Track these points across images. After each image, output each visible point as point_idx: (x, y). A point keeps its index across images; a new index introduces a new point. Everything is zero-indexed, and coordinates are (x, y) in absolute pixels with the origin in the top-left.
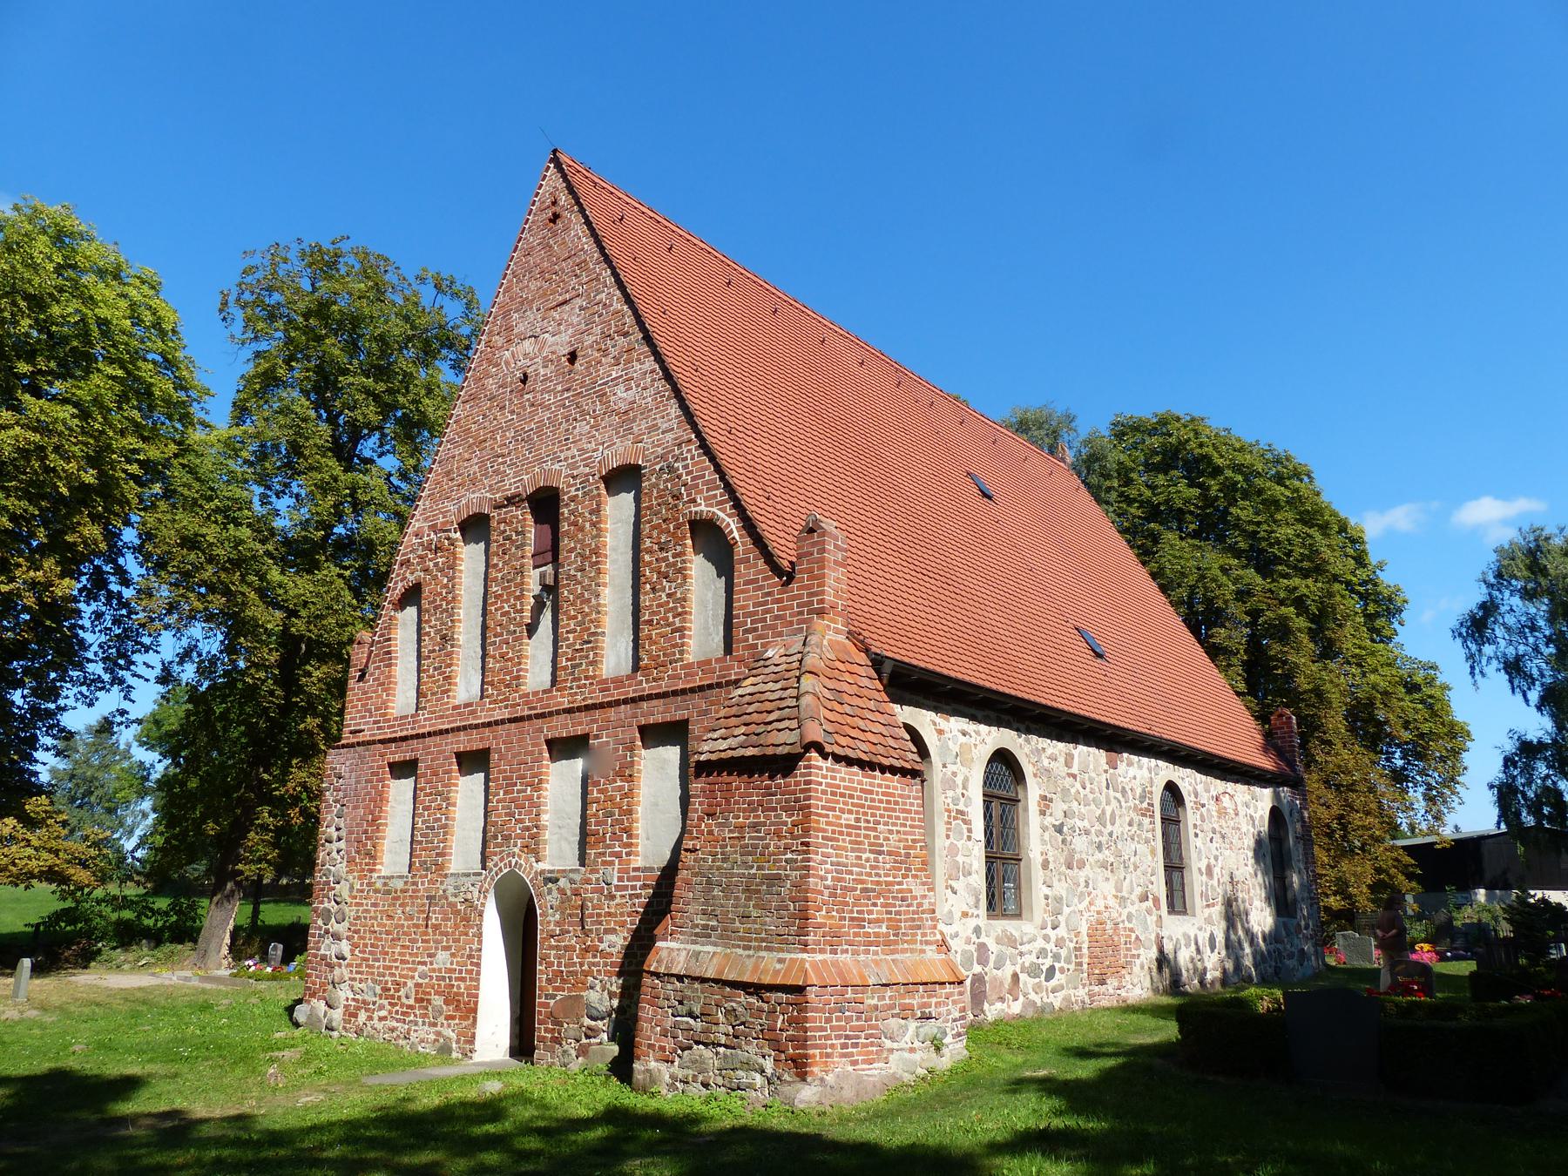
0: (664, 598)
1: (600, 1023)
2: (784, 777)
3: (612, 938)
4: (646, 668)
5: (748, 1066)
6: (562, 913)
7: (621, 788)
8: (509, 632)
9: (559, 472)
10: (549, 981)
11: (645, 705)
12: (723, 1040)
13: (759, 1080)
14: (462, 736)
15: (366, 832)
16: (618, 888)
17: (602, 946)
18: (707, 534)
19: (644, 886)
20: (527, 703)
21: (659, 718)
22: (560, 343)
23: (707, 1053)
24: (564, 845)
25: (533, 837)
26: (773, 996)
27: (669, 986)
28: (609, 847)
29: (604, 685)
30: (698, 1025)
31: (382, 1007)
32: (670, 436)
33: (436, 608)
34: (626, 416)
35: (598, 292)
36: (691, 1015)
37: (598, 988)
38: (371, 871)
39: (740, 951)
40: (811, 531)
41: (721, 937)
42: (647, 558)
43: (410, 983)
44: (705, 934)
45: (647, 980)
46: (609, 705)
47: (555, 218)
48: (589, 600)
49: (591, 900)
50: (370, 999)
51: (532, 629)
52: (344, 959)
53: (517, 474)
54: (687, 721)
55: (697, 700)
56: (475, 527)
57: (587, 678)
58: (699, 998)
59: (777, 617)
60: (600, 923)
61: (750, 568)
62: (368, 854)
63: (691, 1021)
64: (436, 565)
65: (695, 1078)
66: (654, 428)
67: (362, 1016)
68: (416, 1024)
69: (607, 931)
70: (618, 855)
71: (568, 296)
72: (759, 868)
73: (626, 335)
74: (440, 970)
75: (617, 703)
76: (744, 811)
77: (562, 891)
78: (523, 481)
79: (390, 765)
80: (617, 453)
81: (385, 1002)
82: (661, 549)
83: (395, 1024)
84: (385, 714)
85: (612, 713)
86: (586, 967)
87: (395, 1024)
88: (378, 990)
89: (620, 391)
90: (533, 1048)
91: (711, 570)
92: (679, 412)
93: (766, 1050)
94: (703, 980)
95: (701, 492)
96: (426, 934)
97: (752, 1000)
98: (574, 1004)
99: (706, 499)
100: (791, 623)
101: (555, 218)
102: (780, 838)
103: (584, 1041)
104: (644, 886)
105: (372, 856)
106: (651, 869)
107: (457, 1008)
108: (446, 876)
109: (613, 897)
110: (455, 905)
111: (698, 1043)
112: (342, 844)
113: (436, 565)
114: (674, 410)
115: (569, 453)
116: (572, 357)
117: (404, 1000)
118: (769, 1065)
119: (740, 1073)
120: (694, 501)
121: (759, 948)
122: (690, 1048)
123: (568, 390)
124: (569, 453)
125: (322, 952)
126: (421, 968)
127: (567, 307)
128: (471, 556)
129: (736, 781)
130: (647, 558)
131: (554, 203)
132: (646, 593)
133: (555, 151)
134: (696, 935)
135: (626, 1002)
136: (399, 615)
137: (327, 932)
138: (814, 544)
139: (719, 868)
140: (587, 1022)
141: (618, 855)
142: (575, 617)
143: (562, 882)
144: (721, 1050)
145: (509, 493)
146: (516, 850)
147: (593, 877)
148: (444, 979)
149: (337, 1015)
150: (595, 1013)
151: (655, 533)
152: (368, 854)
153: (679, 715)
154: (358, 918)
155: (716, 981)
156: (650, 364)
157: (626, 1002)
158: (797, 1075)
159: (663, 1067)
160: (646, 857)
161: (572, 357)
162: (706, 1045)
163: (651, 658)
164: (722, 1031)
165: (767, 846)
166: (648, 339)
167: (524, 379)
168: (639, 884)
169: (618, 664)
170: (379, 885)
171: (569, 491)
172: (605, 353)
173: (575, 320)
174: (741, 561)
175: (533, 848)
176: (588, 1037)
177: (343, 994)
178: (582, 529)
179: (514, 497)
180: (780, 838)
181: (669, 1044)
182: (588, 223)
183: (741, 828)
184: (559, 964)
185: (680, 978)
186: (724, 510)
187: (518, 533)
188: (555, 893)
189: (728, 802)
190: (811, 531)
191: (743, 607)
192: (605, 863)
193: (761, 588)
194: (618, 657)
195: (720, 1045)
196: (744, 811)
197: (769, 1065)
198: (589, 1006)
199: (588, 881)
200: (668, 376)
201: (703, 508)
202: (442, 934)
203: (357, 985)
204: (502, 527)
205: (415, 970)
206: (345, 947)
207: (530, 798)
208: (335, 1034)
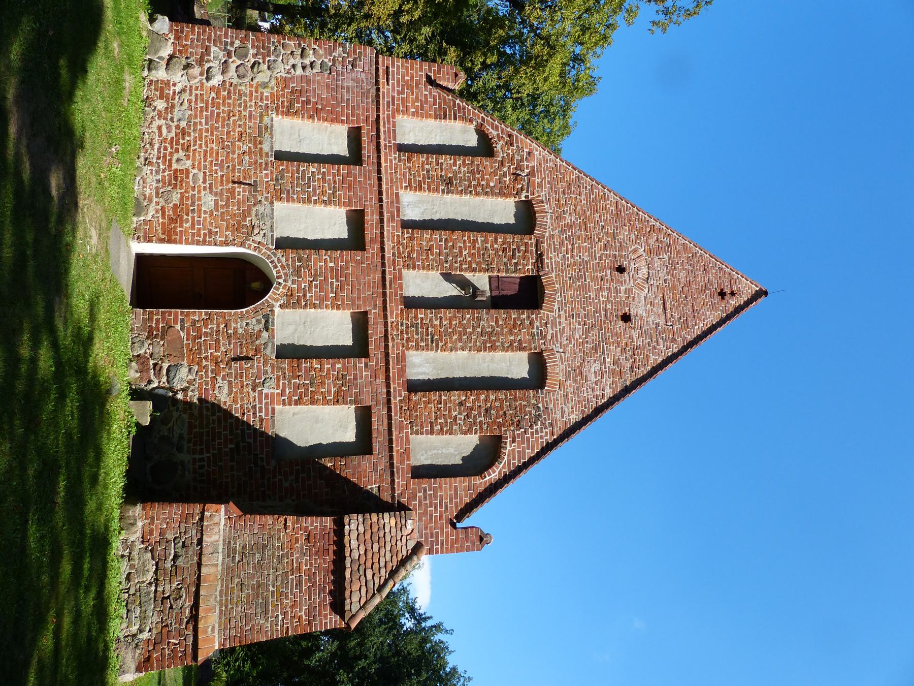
0: (454, 414)
1: (164, 379)
2: (331, 604)
3: (226, 391)
4: (410, 400)
5: (143, 618)
6: (243, 336)
7: (329, 392)
8: (447, 255)
9: (554, 308)
10: (194, 323)
11: (385, 412)
12: (160, 589)
13: (134, 629)
14: (376, 217)
15: (308, 102)
16: (261, 393)
17: (219, 379)
18: (488, 453)
19: (261, 420)
20: (395, 278)
21: (375, 427)
22: (638, 309)
23: (149, 576)
24: (291, 328)
25: (299, 300)
26: (190, 632)
27: (194, 532)
28: (290, 382)
29: (401, 358)
30: (168, 564)
31: (169, 128)
32: (559, 415)
33: (473, 173)
34: (578, 373)
35: (665, 341)
36: (176, 557)
37: (190, 377)
38: (277, 111)
39: (219, 588)
40: (481, 539)
41: (228, 568)
42: (483, 397)
43: (189, 163)
44: (230, 552)
45: (198, 508)
46: (388, 378)
47: (722, 294)
48: (460, 340)
49: (252, 367)
50: (177, 115)
51: (448, 277)
52: (208, 79)
53: (557, 263)
54: (371, 453)
55: (383, 464)
56: (527, 218)
57: (408, 339)
58: (187, 562)
59: (431, 516)
60: (236, 378)
61: (464, 488)
62: (291, 105)
63: (171, 557)
64: (505, 173)
65: (132, 567)
66: (567, 401)
67: (161, 105)
68: (157, 172)
69: (230, 383)
70: (283, 392)
71: (668, 310)
72: (273, 592)
73: (632, 369)
74: (199, 199)
75: (388, 386)
76: (310, 569)
77: (258, 336)
78: (551, 278)
79: (359, 129)
80: (556, 369)
81: (173, 134)
82: (486, 410)
83: (156, 147)
84: (398, 111)
85: (381, 380)
86: (204, 363)
87: (156, 147)
88: (183, 124)
89: (596, 367)
90: (143, 307)
91: (467, 451)
92: (573, 422)
93: (154, 632)
94: (199, 565)
95: (519, 447)
96: (228, 182)
97: (187, 613)
98: (176, 351)
99: (513, 450)
100: (426, 528)
101: (722, 294)
102: (292, 607)
103: (152, 362)
104: (261, 420)
105: (289, 111)
106: (273, 426)
107: (171, 220)
108: (272, 203)
109: (254, 390)
110: (250, 215)
111: (157, 564)
112: (299, 71)
113: (505, 175)
114: (575, 417)
115: (563, 319)
116: (626, 318)
117: (175, 156)
118: (145, 635)
119: (138, 610)
120: (514, 441)
121: (221, 606)
122: (153, 558)
123: (606, 315)
124: (563, 319)
125: (213, 49)
126: (201, 176)
127: (661, 311)
128: (502, 210)
129: (329, 558)
130: (483, 397)
131: (733, 294)
132: (459, 396)
133: (766, 293)
134: (229, 542)
135: (181, 406)
136: (472, 127)
137: (229, 55)
138: (473, 543)
139: (273, 554)
140: (165, 366)
141: (283, 392)
142: (450, 324)
143: (265, 335)
144: (153, 588)
145: (545, 257)
146: (289, 284)
147: (268, 368)
148: (193, 204)
149: (161, 74)
150: (172, 375)
151: (497, 404)
152: (291, 105)
153: (376, 446)
154: (240, 95)
155: (199, 576)
156: (609, 393)
157: (181, 406)
158: (139, 663)
159: (139, 534)
160: (281, 412)
161: (626, 318)
162: (156, 572)
163: (416, 403)
164: (167, 588)
165: (286, 598)
166: (626, 391)
167: (621, 270)
168: (263, 414)
169: (414, 366)
170: (266, 120)
171: (539, 318)
172: (624, 351)
173: (651, 320)
174: (470, 482)
175: (293, 301)
176: (155, 365)
177: (178, 78)
178: (510, 333)
179: (542, 261)
180: (292, 607)
181: (155, 537)
182: (713, 328)
183: (299, 569)
184: (206, 334)
185: (200, 542)
186: (504, 467)
187: (516, 264)
188: (257, 328)
189: (317, 553)
190: (481, 539)
191: (440, 487)
192: (278, 377)
193: (451, 500)
194: (420, 366)
195: (156, 586)
196: (310, 569)
197: (145, 635)
198: (177, 366)
199: (265, 363)
200: (599, 411)
201: (508, 448)
202: (228, 200)
203: (186, 96)
204: (523, 248)
205: (200, 170)
206: (216, 80)
207: (326, 298)
208: (146, 73)
